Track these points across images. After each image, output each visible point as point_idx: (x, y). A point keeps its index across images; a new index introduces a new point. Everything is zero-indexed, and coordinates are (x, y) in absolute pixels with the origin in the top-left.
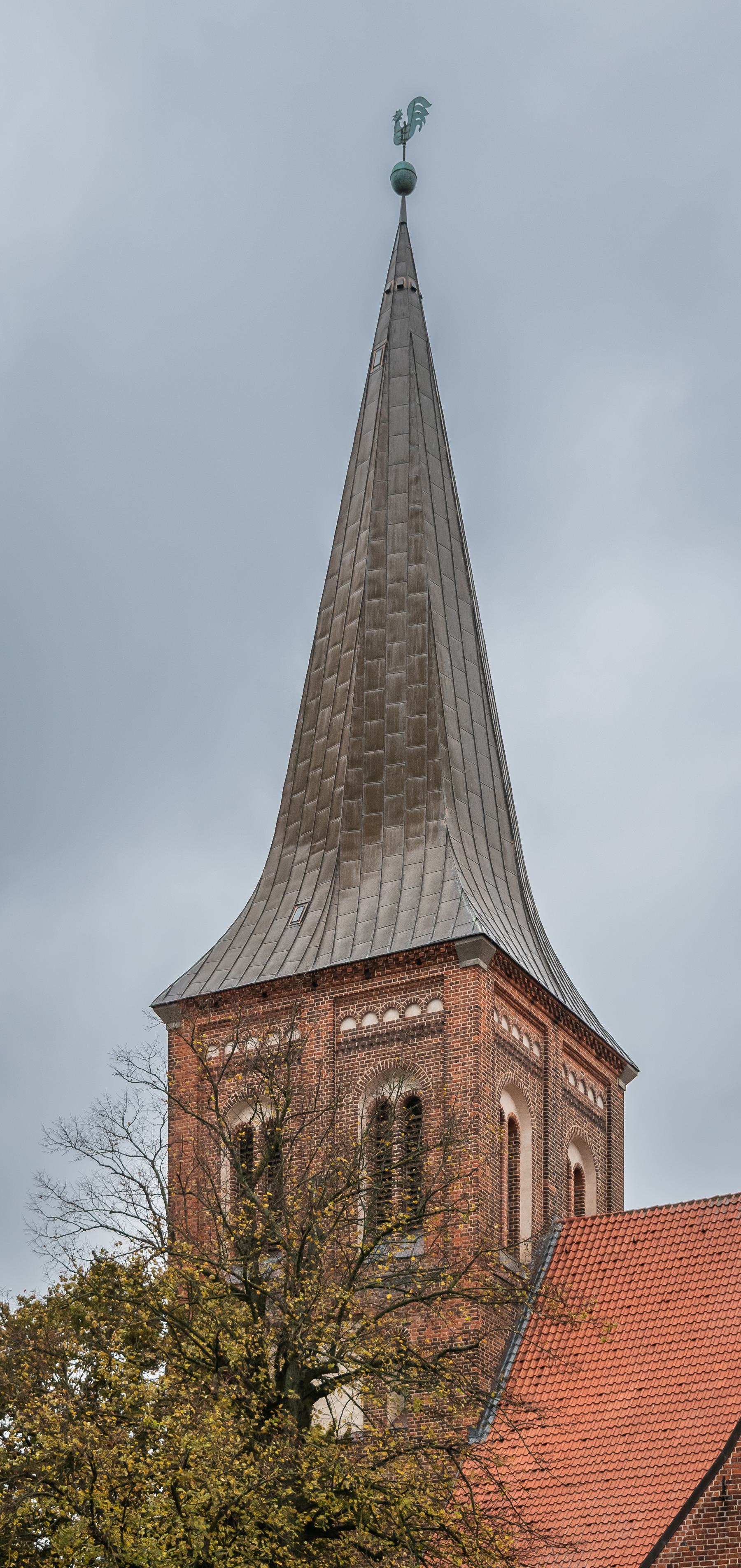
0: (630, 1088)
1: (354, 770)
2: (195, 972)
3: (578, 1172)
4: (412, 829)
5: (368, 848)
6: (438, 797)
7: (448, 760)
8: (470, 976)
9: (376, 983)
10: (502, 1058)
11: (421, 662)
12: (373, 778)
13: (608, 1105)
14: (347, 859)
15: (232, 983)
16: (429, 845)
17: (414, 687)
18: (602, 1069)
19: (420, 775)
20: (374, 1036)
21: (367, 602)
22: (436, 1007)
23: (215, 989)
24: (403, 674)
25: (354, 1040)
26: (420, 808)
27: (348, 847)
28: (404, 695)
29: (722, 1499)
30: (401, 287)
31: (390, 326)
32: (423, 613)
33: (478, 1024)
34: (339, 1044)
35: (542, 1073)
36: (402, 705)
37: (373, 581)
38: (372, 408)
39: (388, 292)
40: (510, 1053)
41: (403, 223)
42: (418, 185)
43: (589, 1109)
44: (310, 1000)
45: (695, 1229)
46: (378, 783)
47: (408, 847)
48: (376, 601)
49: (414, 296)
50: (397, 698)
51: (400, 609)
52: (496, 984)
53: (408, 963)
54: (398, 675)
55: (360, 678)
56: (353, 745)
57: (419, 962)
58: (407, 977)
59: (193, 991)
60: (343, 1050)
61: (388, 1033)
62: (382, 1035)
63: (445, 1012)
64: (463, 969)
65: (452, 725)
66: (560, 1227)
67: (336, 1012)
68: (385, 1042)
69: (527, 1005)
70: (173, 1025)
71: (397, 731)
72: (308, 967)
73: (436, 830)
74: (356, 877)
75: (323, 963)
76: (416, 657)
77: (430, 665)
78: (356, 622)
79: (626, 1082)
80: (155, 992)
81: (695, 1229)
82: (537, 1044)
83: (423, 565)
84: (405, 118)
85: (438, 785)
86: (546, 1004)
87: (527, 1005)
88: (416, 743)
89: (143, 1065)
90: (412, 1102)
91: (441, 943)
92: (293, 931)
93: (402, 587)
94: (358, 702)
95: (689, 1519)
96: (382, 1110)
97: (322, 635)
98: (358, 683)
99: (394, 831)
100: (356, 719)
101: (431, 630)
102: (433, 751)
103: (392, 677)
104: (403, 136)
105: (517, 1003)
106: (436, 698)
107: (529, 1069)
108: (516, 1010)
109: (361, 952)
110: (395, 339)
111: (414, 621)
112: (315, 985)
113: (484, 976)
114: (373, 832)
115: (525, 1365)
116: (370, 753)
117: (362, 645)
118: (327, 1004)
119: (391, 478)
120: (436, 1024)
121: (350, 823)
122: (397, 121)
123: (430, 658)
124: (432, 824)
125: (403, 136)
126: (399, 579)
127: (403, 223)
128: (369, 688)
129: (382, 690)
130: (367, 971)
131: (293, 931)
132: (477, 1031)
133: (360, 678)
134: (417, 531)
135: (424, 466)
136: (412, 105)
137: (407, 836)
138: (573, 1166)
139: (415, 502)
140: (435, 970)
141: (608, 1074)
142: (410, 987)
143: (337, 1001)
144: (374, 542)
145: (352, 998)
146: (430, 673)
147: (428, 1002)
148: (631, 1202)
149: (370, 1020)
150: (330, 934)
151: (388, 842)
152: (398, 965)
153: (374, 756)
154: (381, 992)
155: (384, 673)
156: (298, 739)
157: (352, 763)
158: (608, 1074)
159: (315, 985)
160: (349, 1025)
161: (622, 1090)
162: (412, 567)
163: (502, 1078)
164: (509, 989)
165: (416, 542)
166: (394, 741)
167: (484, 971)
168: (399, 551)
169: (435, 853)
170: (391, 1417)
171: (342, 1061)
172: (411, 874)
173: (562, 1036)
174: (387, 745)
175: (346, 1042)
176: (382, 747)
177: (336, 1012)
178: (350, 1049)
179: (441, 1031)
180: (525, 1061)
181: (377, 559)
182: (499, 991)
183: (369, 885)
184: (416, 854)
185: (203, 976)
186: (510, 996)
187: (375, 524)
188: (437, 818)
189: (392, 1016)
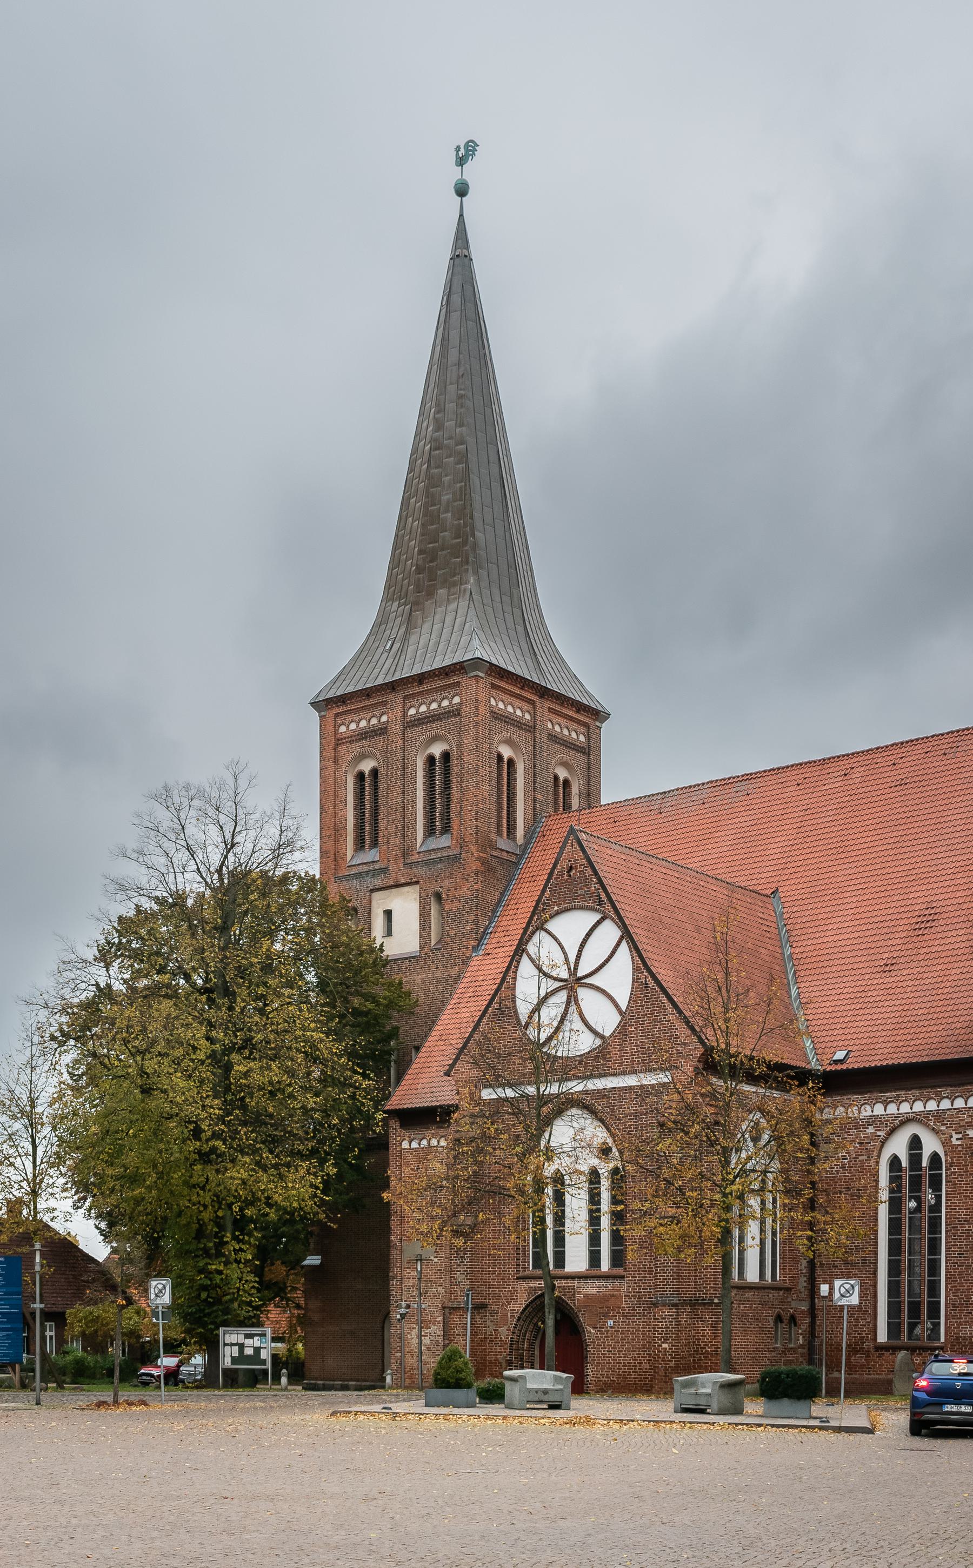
1: (421, 556)
2: (335, 681)
3: (566, 783)
4: (452, 590)
5: (428, 603)
6: (467, 570)
7: (475, 547)
8: (473, 681)
9: (425, 687)
10: (499, 725)
11: (461, 487)
12: (431, 561)
13: (588, 738)
14: (415, 611)
15: (351, 689)
16: (460, 600)
17: (456, 504)
18: (582, 718)
19: (457, 558)
20: (425, 718)
21: (432, 453)
22: (457, 700)
24: (450, 496)
25: (415, 720)
26: (457, 578)
27: (416, 604)
28: (450, 509)
29: (500, 1009)
30: (458, 256)
31: (451, 280)
32: (463, 458)
33: (477, 710)
34: (407, 723)
35: (530, 728)
36: (450, 514)
37: (436, 440)
38: (441, 330)
39: (451, 259)
40: (505, 722)
41: (461, 215)
42: (470, 191)
43: (572, 744)
44: (391, 697)
46: (434, 564)
47: (449, 602)
48: (437, 452)
49: (466, 260)
50: (446, 511)
51: (450, 456)
52: (492, 684)
53: (441, 675)
54: (448, 497)
55: (427, 500)
56: (421, 541)
57: (446, 674)
58: (441, 683)
59: (330, 695)
60: (409, 727)
61: (432, 716)
62: (429, 717)
63: (461, 704)
64: (470, 678)
65: (478, 524)
66: (543, 820)
67: (405, 704)
68: (430, 721)
69: (518, 691)
70: (322, 714)
71: (446, 531)
72: (389, 679)
73: (465, 590)
74: (420, 622)
75: (397, 677)
76: (458, 485)
77: (465, 490)
78: (426, 465)
79: (602, 722)
80: (311, 696)
82: (528, 712)
83: (464, 429)
84: (462, 152)
85: (467, 563)
86: (532, 688)
87: (518, 691)
88: (456, 538)
89: (148, 818)
90: (446, 756)
91: (456, 664)
92: (385, 655)
93: (452, 442)
94: (425, 515)
95: (485, 1020)
96: (431, 760)
97: (411, 473)
98: (425, 502)
99: (442, 592)
100: (424, 525)
101: (467, 469)
102: (465, 542)
103: (445, 498)
104: (461, 162)
105: (510, 691)
106: (468, 511)
107: (521, 728)
108: (510, 695)
109: (417, 670)
110: (454, 288)
111: (458, 463)
112: (393, 689)
113: (481, 681)
114: (431, 593)
115: (509, 908)
116: (431, 545)
117: (428, 480)
118: (400, 700)
119: (448, 375)
120: (457, 710)
121: (418, 589)
122: (457, 152)
123: (465, 485)
124: (463, 587)
125: (461, 162)
126: (450, 438)
127: (461, 215)
128: (432, 506)
129: (438, 506)
130: (420, 680)
131: (385, 655)
132: (477, 714)
133: (427, 500)
134: (462, 407)
135: (468, 366)
136: (467, 145)
137: (448, 595)
138: (561, 779)
139: (461, 390)
140: (455, 679)
141: (587, 720)
143: (405, 698)
144: (437, 416)
145: (413, 696)
146: (465, 495)
147: (453, 697)
148: (606, 798)
149: (423, 708)
150: (403, 657)
151: (438, 599)
152: (436, 676)
153: (433, 547)
154: (428, 692)
155: (440, 495)
156: (396, 536)
157: (421, 552)
158: (587, 720)
159: (393, 689)
160: (412, 711)
161: (600, 728)
162: (458, 430)
163: (497, 738)
164: (503, 684)
165: (461, 413)
166: (444, 537)
167: (482, 678)
168: (451, 420)
169: (463, 604)
170: (433, 943)
171: (409, 733)
172: (449, 619)
173: (547, 704)
174: (440, 540)
175: (411, 721)
176: (437, 542)
177: (405, 704)
178: (413, 726)
179: (459, 714)
180: (518, 724)
181: (439, 426)
182: (494, 686)
183: (427, 626)
184: (453, 606)
185: (337, 685)
186: (504, 688)
187: (438, 405)
188: (466, 583)
189: (434, 706)
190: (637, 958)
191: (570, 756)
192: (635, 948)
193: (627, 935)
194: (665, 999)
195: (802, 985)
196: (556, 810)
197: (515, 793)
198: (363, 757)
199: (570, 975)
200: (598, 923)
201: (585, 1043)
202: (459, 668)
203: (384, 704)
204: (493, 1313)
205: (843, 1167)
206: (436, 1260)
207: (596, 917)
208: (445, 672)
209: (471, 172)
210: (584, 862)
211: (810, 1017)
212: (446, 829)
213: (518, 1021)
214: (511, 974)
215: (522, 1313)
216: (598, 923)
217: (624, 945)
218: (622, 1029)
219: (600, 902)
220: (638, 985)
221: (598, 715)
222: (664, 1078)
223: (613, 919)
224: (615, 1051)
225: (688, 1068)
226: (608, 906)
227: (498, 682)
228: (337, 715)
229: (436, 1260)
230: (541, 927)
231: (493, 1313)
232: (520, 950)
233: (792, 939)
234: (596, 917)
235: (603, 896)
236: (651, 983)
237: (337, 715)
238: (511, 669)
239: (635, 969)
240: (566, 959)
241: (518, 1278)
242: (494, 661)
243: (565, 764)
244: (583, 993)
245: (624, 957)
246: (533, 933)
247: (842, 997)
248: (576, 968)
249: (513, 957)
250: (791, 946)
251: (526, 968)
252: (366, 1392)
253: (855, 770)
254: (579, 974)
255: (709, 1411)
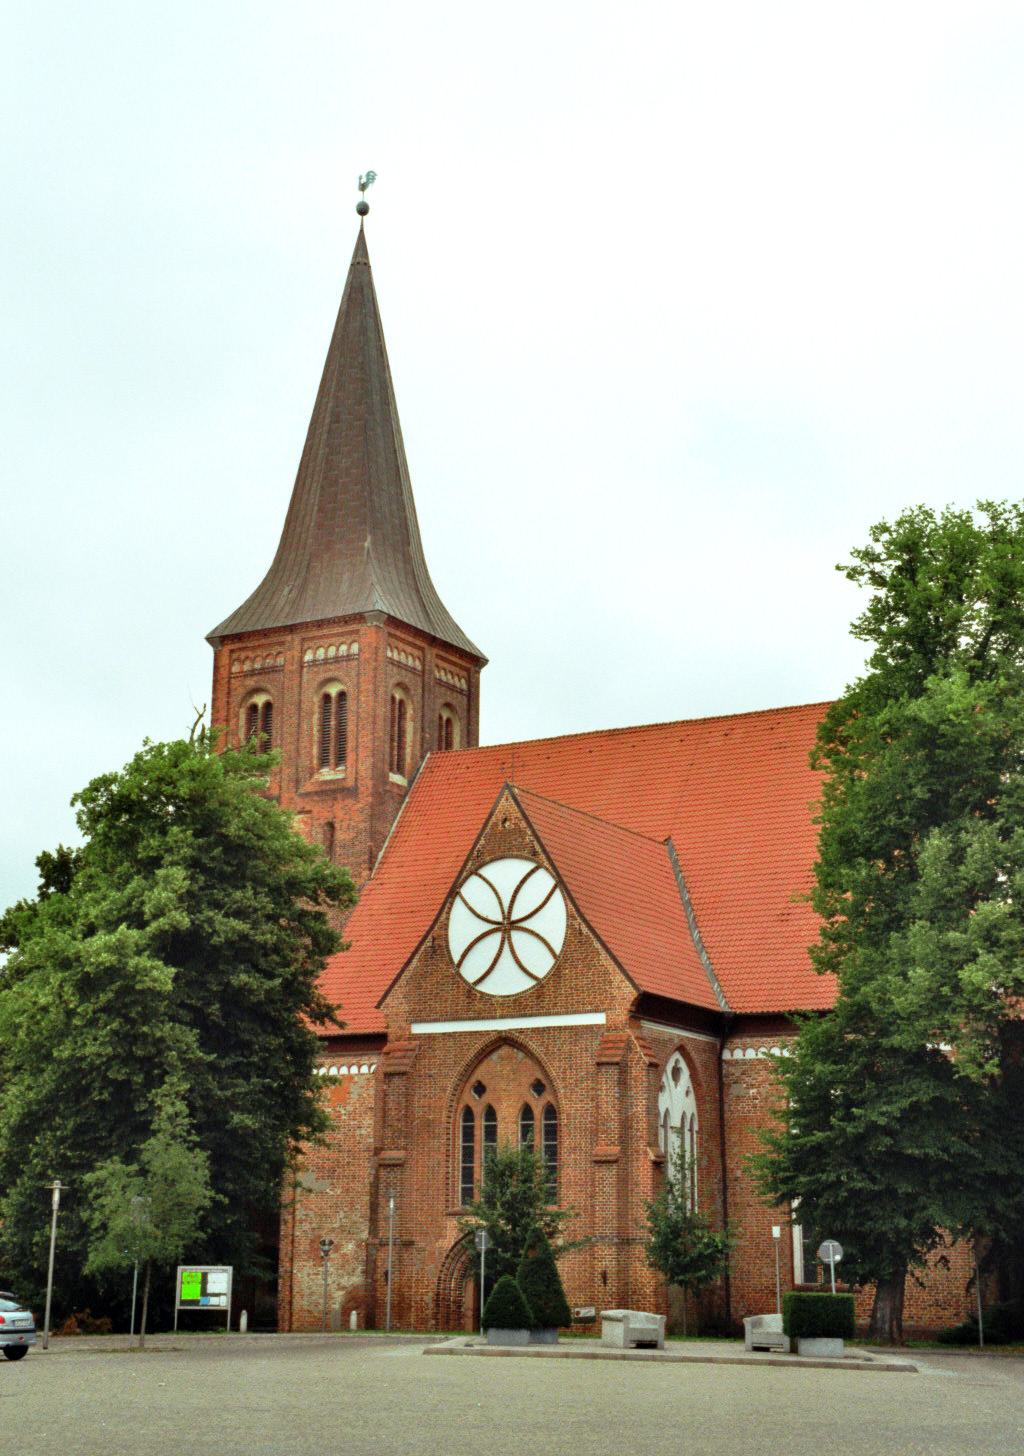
0: (485, 675)
3: (401, 702)
9: (325, 631)
23: (239, 631)
30: (358, 263)
41: (362, 225)
45: (500, 762)
57: (346, 622)
59: (226, 633)
67: (302, 645)
80: (208, 630)
81: (500, 762)
82: (419, 658)
87: (411, 639)
95: (417, 957)
104: (363, 187)
127: (362, 231)
136: (368, 174)
138: (445, 718)
140: (355, 627)
142: (342, 634)
164: (398, 633)
173: (435, 651)
190: (571, 906)
191: (450, 697)
192: (569, 896)
193: (560, 883)
194: (597, 945)
195: (703, 929)
196: (440, 749)
197: (404, 732)
198: (257, 690)
199: (504, 919)
200: (533, 872)
201: (521, 984)
202: (359, 618)
203: (282, 643)
204: (421, 1250)
205: (755, 1106)
206: (332, 1193)
207: (530, 866)
208: (346, 620)
209: (369, 197)
210: (519, 815)
211: (715, 961)
212: (341, 758)
213: (451, 959)
214: (444, 915)
215: (451, 1250)
216: (533, 872)
217: (558, 894)
218: (556, 972)
219: (535, 853)
220: (572, 933)
221: (477, 661)
222: (599, 1019)
223: (547, 869)
224: (550, 989)
225: (622, 1014)
226: (542, 857)
227: (393, 631)
228: (232, 651)
229: (332, 1193)
230: (475, 872)
231: (421, 1250)
232: (454, 892)
233: (688, 885)
234: (530, 866)
235: (538, 848)
236: (585, 930)
237: (232, 651)
238: (405, 620)
239: (570, 916)
240: (501, 904)
241: (447, 1215)
242: (392, 614)
243: (448, 705)
244: (516, 936)
245: (558, 904)
246: (467, 878)
247: (743, 943)
248: (510, 912)
249: (447, 898)
250: (689, 892)
251: (458, 910)
252: (304, 1335)
253: (735, 732)
254: (515, 916)
255: (772, 1350)
